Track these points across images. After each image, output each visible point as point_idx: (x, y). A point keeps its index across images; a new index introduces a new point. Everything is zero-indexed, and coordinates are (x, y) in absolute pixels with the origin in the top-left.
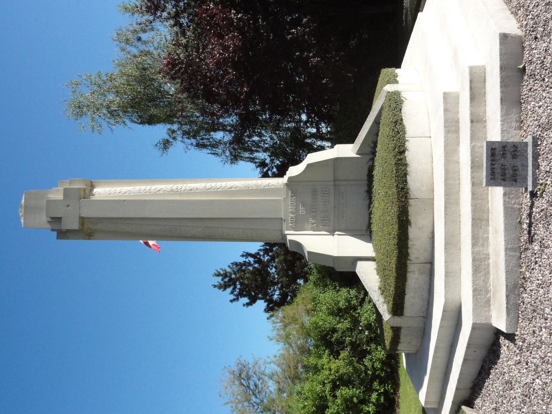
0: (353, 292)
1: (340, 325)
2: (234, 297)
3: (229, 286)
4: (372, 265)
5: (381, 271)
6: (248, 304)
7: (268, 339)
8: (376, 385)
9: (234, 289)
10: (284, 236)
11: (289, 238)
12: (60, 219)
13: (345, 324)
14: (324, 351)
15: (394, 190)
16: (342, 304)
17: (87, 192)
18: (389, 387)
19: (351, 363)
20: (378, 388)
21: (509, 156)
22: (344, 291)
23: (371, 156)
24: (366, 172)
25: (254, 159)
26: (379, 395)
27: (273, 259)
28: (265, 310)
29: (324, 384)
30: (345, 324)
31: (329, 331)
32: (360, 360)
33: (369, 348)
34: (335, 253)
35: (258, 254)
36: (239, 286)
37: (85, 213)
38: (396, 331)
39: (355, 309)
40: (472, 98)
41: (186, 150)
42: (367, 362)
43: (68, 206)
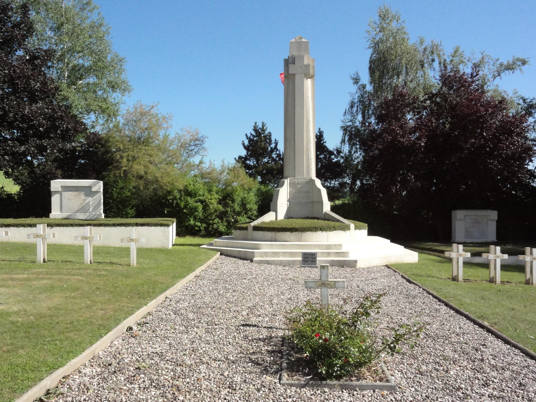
0: (255, 213)
1: (236, 205)
2: (249, 137)
3: (256, 133)
4: (274, 219)
5: (271, 222)
6: (244, 144)
7: (222, 160)
8: (204, 225)
9: (254, 136)
10: (286, 178)
11: (286, 180)
12: (294, 63)
13: (237, 208)
14: (221, 196)
15: (305, 226)
16: (248, 206)
17: (308, 76)
18: (203, 232)
19: (216, 211)
20: (203, 226)
21: (312, 260)
22: (255, 207)
23: (323, 219)
24: (316, 216)
25: (344, 142)
26: (199, 227)
27: (274, 160)
28: (240, 156)
29: (203, 195)
30: (237, 208)
31: (233, 198)
32: (217, 216)
33: (224, 221)
34: (279, 202)
35: (277, 150)
36: (255, 139)
37: (297, 77)
38: (246, 229)
39: (246, 214)
40: (337, 253)
41: (350, 94)
42: (216, 220)
43: (301, 67)
